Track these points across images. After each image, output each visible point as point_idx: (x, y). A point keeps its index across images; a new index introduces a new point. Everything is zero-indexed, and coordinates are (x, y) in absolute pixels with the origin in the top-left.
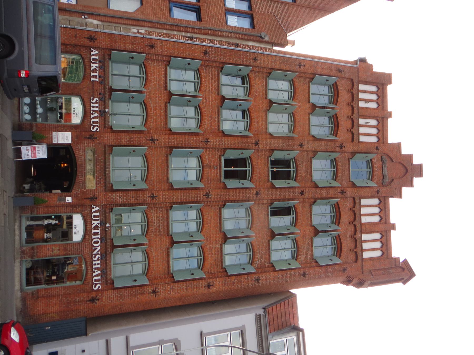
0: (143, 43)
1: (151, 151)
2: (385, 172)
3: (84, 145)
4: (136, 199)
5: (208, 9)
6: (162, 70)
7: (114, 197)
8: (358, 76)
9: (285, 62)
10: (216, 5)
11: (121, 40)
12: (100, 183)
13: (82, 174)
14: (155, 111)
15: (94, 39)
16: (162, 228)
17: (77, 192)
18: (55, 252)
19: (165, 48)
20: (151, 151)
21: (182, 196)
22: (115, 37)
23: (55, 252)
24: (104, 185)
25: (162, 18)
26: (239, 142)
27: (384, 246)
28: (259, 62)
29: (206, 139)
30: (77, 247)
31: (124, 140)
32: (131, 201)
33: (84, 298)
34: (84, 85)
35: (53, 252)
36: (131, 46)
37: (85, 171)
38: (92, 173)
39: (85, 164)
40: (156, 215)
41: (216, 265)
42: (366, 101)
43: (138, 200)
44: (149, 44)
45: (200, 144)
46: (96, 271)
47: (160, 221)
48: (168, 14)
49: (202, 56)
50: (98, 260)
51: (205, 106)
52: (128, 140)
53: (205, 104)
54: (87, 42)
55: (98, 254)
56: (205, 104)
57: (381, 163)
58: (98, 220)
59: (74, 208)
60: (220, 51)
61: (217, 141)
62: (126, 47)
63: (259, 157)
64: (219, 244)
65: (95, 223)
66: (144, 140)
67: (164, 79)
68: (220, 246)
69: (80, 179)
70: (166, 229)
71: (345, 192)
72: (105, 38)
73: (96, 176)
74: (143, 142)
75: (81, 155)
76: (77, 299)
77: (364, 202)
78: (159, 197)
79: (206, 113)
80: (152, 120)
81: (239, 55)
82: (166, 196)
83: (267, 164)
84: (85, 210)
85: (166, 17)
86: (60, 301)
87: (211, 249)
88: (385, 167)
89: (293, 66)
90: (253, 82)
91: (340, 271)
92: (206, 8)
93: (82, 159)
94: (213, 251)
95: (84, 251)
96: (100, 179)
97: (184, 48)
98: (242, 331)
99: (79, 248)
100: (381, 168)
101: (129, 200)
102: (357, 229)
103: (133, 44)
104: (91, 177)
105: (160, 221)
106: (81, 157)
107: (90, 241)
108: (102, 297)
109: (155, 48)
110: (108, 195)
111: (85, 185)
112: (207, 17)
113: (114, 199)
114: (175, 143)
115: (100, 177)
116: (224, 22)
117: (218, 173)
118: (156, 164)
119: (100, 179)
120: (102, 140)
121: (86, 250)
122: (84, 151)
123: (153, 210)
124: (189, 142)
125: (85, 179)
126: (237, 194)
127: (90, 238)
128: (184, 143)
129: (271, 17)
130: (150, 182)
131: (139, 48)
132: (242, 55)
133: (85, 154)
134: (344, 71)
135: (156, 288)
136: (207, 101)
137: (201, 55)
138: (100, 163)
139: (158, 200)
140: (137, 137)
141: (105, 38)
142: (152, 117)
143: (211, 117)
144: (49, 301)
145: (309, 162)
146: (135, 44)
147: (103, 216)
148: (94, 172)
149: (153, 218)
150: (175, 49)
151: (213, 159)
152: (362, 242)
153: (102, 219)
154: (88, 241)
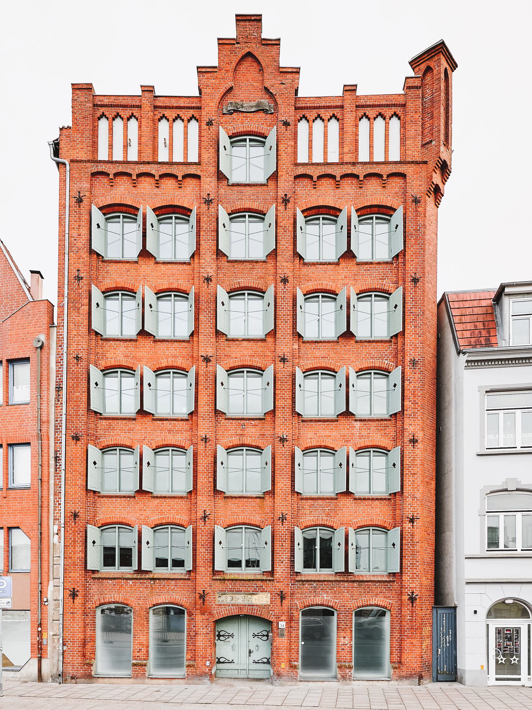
4: (285, 541)
7: (281, 570)
12: (262, 586)
16: (327, 507)
17: (274, 615)
19: (75, 498)
20: (220, 520)
21: (284, 478)
26: (206, 389)
28: (81, 352)
29: (202, 440)
30: (343, 616)
31: (206, 555)
35: (346, 645)
36: (78, 544)
37: (246, 605)
38: (250, 596)
39: (238, 605)
43: (285, 539)
45: (209, 450)
47: (317, 510)
51: (153, 440)
52: (206, 550)
56: (151, 440)
62: (80, 551)
64: (355, 423)
67: (119, 499)
68: (358, 423)
69: (257, 611)
70: (327, 501)
72: (70, 577)
76: (409, 618)
80: (177, 516)
81: (73, 385)
83: (238, 343)
84: (297, 606)
89: (80, 291)
90: (113, 363)
91: (416, 211)
94: (364, 433)
96: (257, 587)
99: (345, 613)
100: (244, 115)
105: (317, 510)
109: (77, 511)
110: (278, 577)
113: (283, 570)
117: (251, 423)
118: (237, 513)
119: (257, 587)
120: (205, 584)
121: (347, 606)
122: (220, 605)
125: (257, 605)
132: (73, 380)
134: (79, 192)
139: (287, 512)
141: (70, 577)
142: (173, 517)
143: (170, 431)
146: (74, 539)
149: (311, 518)
150: (76, 483)
154: (336, 602)
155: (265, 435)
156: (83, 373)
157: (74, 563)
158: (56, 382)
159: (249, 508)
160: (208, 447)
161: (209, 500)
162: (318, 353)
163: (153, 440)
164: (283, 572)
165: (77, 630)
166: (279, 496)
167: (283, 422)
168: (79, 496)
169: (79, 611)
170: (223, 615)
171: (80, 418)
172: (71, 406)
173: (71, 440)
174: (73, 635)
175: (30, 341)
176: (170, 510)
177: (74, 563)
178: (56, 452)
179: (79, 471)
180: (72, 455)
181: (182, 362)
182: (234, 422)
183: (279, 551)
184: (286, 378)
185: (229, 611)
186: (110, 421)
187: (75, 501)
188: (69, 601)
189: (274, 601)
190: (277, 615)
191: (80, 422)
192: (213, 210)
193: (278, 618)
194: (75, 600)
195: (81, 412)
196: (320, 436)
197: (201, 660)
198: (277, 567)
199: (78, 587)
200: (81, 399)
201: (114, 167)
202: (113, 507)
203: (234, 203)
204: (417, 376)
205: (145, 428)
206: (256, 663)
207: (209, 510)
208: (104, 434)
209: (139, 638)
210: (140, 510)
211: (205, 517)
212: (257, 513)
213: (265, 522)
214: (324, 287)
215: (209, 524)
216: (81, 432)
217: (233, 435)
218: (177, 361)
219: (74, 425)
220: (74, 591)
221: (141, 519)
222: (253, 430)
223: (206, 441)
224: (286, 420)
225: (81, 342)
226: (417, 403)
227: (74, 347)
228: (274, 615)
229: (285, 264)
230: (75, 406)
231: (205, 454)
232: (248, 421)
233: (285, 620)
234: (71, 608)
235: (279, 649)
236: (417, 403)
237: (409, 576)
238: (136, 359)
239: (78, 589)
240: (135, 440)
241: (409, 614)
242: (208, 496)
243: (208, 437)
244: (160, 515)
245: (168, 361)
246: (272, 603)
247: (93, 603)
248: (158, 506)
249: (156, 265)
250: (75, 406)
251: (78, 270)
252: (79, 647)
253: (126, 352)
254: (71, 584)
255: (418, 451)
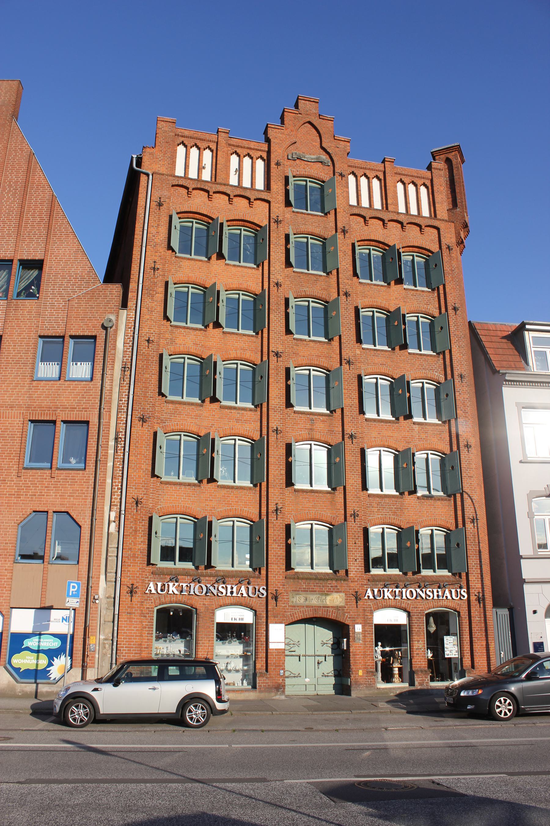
0: (134, 515)
1: (291, 514)
2: (312, 159)
3: (286, 606)
4: (358, 539)
5: (68, 408)
6: (170, 490)
7: (354, 569)
8: (167, 175)
9: (150, 294)
10: (58, 395)
11: (131, 548)
12: (337, 586)
13: (325, 610)
14: (231, 504)
15: (132, 587)
16: (393, 506)
17: (349, 618)
18: (421, 646)
19: (139, 483)
20: (291, 514)
21: (354, 475)
22: (128, 557)
23: (421, 646)
24: (339, 582)
25: (88, 482)
26: (277, 382)
27: (251, 153)
29: (273, 432)
30: (416, 618)
31: (278, 551)
32: (360, 546)
33: (476, 610)
34: (200, 604)
35: (420, 649)
36: (139, 533)
37: (321, 607)
38: (324, 597)
39: (312, 607)
40: (376, 512)
41: (440, 434)
42: (200, 168)
43: (358, 536)
44: (135, 507)
45: (281, 442)
46: (445, 595)
47: (384, 508)
48: (79, 474)
49: (148, 426)
50: (433, 592)
51: (221, 428)
52: (278, 546)
53: (219, 427)
54: (137, 598)
55: (426, 592)
56: (219, 427)
57: (298, 161)
58: (384, 591)
59: (367, 621)
60: (138, 396)
61: (276, 416)
62: (142, 542)
63: (296, 354)
64: (414, 426)
65: (387, 594)
66: (278, 523)
67: (183, 487)
68: (417, 426)
69: (332, 614)
70: (393, 499)
71: (344, 227)
72: (129, 571)
73: (327, 591)
74: (280, 525)
75: (300, 611)
76: (478, 619)
77: (179, 171)
78: (355, 507)
79: (232, 428)
80: (245, 509)
81: (143, 366)
82: (353, 497)
84: (371, 608)
85: (85, 477)
86: (479, 640)
87: (420, 439)
88: (304, 157)
89: (156, 280)
90: (182, 349)
91: (450, 256)
92: (66, 411)
93: (305, 611)
94: (423, 436)
95: (421, 610)
96: (331, 586)
97: (138, 454)
98: (523, 408)
99: (417, 615)
100: (306, 163)
101: (358, 549)
102: (395, 218)
103: (136, 531)
104: (328, 598)
105: (384, 508)
106: (303, 611)
107: (409, 602)
108: (476, 588)
109: (140, 498)
110: (353, 577)
111: (340, 607)
112: (82, 411)
114: (281, 479)
115: (328, 586)
116: (88, 385)
117: (319, 419)
118: (308, 508)
119: (331, 586)
120: (278, 582)
121: (419, 608)
122: (294, 606)
123: (369, 516)
124: (279, 458)
125: (332, 607)
126: (351, 394)
127: (405, 601)
128: (280, 465)
129: (74, 305)
130: (334, 517)
131: (142, 523)
132: (142, 362)
133: (298, 606)
134: (160, 198)
135: (469, 518)
136: (214, 425)
137: (146, 428)
138: (311, 586)
139: (358, 509)
140: (274, 533)
142: (241, 510)
143: (238, 420)
144: (478, 653)
145: (300, 276)
146: (136, 528)
147: (378, 585)
148: (322, 595)
149: (379, 516)
150: (140, 467)
151: (299, 424)
152: (199, 180)
153: (381, 585)
154: (408, 604)
155: (333, 431)
156: (154, 356)
157: (134, 555)
158: (123, 362)
159: (320, 504)
160: (280, 439)
161: (281, 493)
162: (376, 360)
163: (221, 428)
164: (357, 571)
165: (134, 633)
166: (350, 493)
167: (351, 420)
168: (143, 481)
169: (137, 610)
170: (297, 617)
171: (148, 399)
172: (139, 386)
173: (137, 422)
174: (130, 639)
175: (98, 320)
176: (238, 502)
177: (134, 555)
178: (117, 433)
179: (144, 454)
180: (138, 437)
181: (250, 355)
182: (303, 416)
183: (353, 549)
184: (352, 379)
185: (303, 613)
186: (177, 405)
187: (138, 486)
188: (126, 599)
189: (350, 602)
190: (353, 618)
191: (148, 404)
192: (281, 229)
193: (354, 621)
194: (134, 598)
195: (149, 394)
196: (383, 436)
197: (274, 669)
198: (351, 566)
199: (137, 582)
200: (150, 381)
201: (193, 184)
202: (177, 495)
203: (299, 226)
204: (465, 389)
205: (213, 415)
206: (325, 676)
207: (281, 503)
208: (169, 418)
209: (204, 643)
210: (206, 500)
211: (277, 510)
212: (328, 509)
213: (336, 518)
214: (379, 304)
215: (282, 518)
216: (149, 414)
217: (303, 428)
218: (246, 354)
219: (141, 406)
220: (132, 587)
221: (207, 510)
222: (322, 425)
223: (277, 433)
224: (354, 418)
225: (154, 327)
226: (467, 413)
227: (145, 330)
228: (349, 618)
229: (346, 281)
230: (143, 387)
231: (277, 446)
232: (316, 417)
233: (360, 624)
234: (129, 607)
235: (356, 655)
236: (467, 413)
237: (475, 576)
238: (206, 347)
239: (138, 584)
240: (202, 426)
241: (477, 615)
242: (280, 488)
243: (279, 429)
244: (227, 506)
245: (236, 353)
246: (347, 605)
247: (152, 603)
248: (224, 496)
249: (227, 267)
250: (143, 387)
251: (155, 262)
252: (135, 653)
253: (195, 340)
254: (130, 579)
255: (472, 456)
